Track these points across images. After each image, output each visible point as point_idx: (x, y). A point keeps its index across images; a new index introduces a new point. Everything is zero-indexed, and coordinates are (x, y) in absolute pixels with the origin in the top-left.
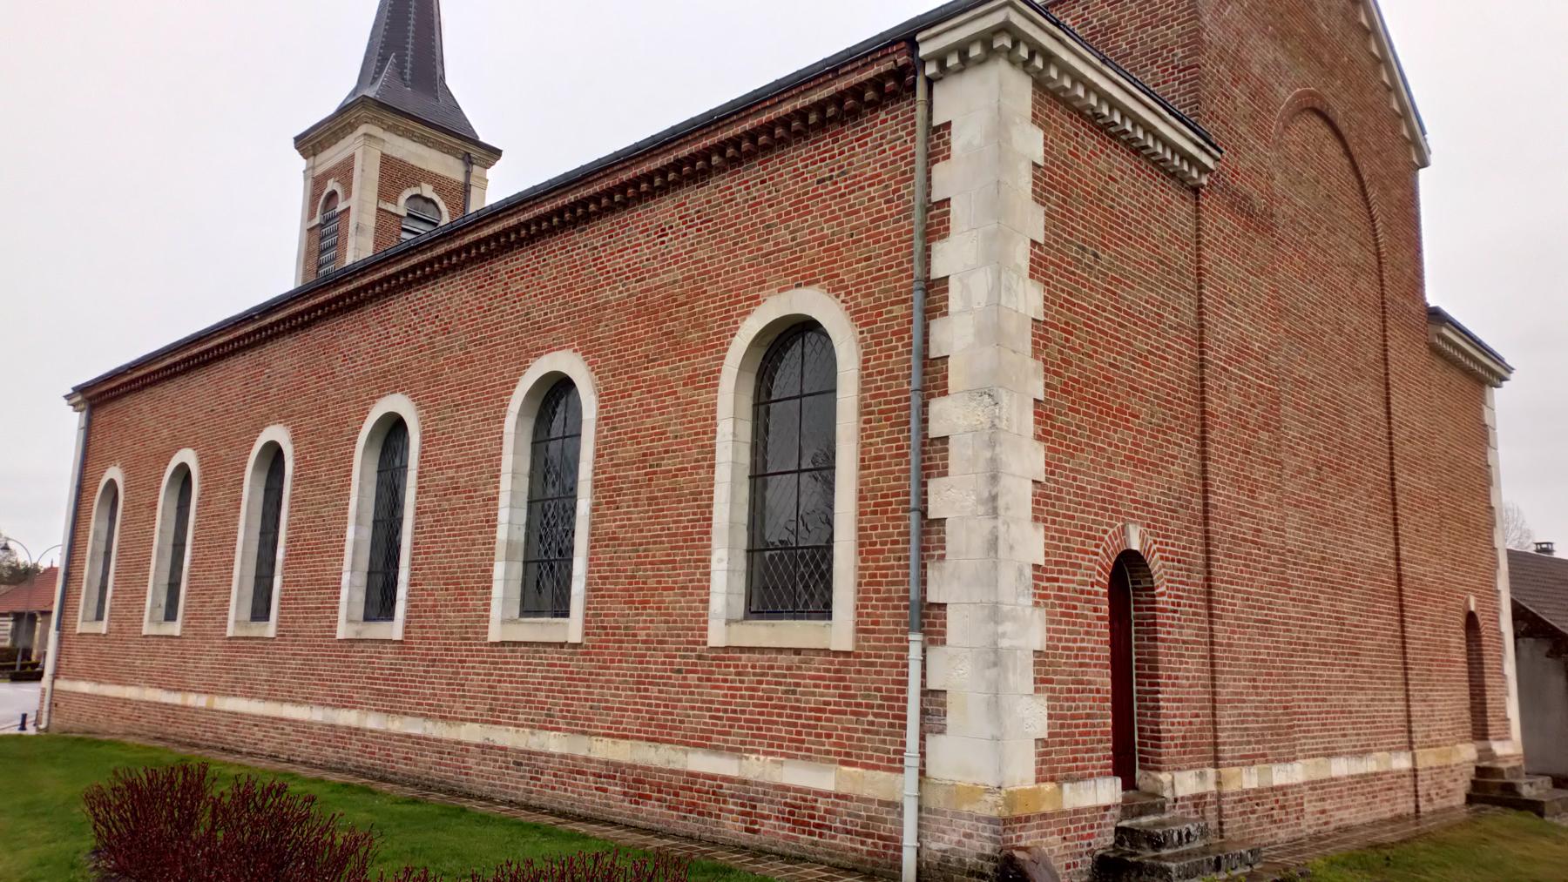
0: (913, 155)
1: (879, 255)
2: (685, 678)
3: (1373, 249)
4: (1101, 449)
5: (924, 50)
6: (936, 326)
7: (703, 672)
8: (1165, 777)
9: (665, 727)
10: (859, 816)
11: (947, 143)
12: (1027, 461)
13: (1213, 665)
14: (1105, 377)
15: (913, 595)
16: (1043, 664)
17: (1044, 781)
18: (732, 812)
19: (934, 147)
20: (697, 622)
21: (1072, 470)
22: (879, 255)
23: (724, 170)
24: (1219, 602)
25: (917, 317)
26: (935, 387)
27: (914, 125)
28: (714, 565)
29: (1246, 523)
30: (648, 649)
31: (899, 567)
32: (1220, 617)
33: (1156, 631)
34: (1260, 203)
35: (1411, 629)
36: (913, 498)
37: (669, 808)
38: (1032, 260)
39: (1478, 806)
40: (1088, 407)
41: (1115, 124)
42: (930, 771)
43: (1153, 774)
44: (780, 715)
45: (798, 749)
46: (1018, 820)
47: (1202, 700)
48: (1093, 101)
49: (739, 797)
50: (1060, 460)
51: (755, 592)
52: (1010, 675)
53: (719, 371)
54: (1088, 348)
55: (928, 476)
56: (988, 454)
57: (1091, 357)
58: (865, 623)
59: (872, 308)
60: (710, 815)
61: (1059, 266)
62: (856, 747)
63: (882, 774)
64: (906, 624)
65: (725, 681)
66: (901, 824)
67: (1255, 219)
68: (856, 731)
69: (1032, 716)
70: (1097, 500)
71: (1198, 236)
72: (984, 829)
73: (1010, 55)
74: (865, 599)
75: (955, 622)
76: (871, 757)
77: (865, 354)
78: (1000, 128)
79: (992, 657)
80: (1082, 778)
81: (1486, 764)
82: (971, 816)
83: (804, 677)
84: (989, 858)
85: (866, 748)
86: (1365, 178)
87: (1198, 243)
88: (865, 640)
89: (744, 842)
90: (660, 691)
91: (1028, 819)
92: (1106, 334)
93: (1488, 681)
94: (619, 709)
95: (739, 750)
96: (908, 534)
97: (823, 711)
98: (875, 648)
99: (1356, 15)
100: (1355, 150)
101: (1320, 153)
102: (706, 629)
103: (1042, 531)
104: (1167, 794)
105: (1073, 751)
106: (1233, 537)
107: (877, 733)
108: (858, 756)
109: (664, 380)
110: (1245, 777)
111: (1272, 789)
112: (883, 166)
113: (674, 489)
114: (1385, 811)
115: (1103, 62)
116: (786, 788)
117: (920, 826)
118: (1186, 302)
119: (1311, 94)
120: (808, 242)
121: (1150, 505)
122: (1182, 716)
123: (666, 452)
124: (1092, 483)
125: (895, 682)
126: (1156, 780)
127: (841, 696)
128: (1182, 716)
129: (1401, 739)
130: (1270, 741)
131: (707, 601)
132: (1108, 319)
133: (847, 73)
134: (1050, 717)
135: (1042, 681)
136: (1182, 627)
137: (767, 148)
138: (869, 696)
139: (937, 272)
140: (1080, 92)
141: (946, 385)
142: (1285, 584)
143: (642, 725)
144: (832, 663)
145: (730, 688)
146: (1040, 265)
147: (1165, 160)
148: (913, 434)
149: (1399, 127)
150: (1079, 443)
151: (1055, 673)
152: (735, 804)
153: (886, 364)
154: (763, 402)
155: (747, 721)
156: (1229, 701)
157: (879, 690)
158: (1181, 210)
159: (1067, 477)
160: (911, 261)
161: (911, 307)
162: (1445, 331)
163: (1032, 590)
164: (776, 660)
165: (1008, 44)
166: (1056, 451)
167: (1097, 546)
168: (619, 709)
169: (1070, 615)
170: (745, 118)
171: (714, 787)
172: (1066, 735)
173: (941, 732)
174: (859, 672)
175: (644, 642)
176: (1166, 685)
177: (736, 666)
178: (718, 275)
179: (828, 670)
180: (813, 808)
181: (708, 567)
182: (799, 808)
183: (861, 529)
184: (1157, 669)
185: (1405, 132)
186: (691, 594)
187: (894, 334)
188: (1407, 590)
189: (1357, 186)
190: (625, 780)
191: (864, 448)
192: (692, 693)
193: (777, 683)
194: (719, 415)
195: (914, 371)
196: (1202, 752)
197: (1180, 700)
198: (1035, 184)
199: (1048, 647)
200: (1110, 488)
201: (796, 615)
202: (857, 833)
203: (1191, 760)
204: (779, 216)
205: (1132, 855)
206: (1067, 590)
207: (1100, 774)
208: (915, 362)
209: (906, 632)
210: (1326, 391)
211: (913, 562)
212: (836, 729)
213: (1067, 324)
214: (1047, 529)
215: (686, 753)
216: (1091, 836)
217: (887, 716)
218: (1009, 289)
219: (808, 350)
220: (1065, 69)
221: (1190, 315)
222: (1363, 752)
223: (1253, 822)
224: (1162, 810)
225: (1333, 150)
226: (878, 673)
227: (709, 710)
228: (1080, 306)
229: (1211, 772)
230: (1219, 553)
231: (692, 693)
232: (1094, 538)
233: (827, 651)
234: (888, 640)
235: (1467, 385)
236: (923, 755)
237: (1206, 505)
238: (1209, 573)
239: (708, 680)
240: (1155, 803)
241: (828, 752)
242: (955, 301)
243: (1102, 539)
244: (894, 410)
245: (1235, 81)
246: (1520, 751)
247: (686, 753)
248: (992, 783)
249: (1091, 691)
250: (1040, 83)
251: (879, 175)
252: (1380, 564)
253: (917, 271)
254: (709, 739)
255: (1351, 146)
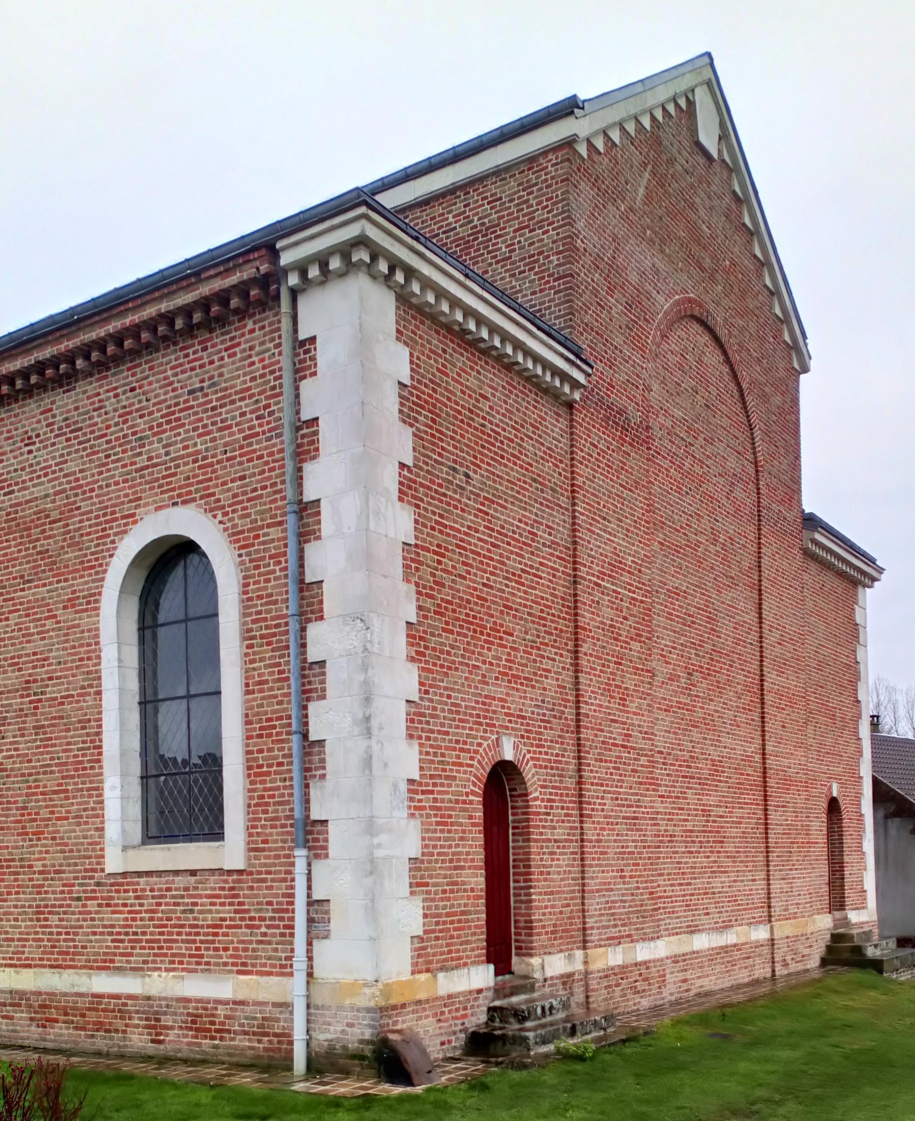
0: (280, 369)
1: (254, 475)
2: (84, 906)
3: (750, 457)
4: (475, 667)
5: (286, 259)
6: (312, 550)
7: (103, 898)
8: (535, 961)
9: (67, 953)
10: (255, 1018)
11: (313, 359)
12: (401, 682)
13: (582, 859)
14: (478, 597)
15: (297, 814)
16: (419, 869)
17: (420, 972)
18: (137, 1026)
19: (300, 362)
20: (94, 850)
21: (446, 689)
22: (254, 475)
23: (91, 375)
24: (589, 803)
25: (292, 541)
26: (312, 612)
27: (280, 337)
28: (107, 793)
29: (617, 729)
30: (45, 879)
31: (285, 787)
32: (590, 816)
33: (529, 833)
34: (635, 416)
35: (773, 817)
36: (294, 721)
37: (76, 1028)
38: (401, 483)
39: (830, 967)
40: (461, 627)
41: (483, 340)
42: (317, 972)
43: (526, 959)
44: (179, 934)
45: (198, 963)
46: (394, 1007)
47: (573, 891)
48: (459, 317)
49: (144, 1012)
50: (434, 679)
51: (152, 818)
52: (387, 883)
53: (100, 594)
54: (461, 570)
55: (308, 700)
56: (362, 678)
57: (464, 578)
58: (256, 842)
59: (249, 530)
60: (117, 1031)
61: (429, 488)
62: (250, 957)
63: (274, 979)
64: (293, 841)
65: (125, 905)
66: (292, 1020)
67: (633, 433)
68: (251, 942)
69: (408, 916)
70: (471, 715)
71: (572, 453)
72: (364, 1018)
73: (370, 268)
74: (255, 819)
75: (336, 836)
76: (265, 965)
77: (245, 578)
78: (363, 343)
79: (368, 867)
80: (457, 967)
81: (841, 931)
82: (352, 1008)
83: (200, 896)
84: (368, 1042)
85: (260, 957)
86: (744, 386)
87: (572, 459)
88: (256, 858)
89: (151, 1052)
90: (61, 920)
91: (403, 1006)
92: (479, 554)
93: (846, 859)
94: (19, 940)
95: (142, 969)
96: (290, 756)
97: (221, 927)
98: (265, 865)
99: (740, 216)
100: (735, 357)
101: (700, 361)
102: (103, 857)
103: (417, 748)
104: (537, 975)
105: (448, 945)
106: (603, 743)
107: (270, 943)
108: (253, 965)
109: (42, 603)
110: (610, 956)
111: (636, 964)
112: (253, 379)
113: (62, 718)
114: (743, 976)
115: (466, 276)
116: (187, 1000)
117: (308, 1021)
118: (560, 520)
119: (690, 300)
120: (182, 457)
121: (524, 718)
122: (553, 907)
123: (50, 679)
124: (466, 700)
125: (284, 895)
126: (528, 964)
127: (236, 912)
128: (553, 907)
129: (762, 913)
130: (635, 924)
131: (102, 829)
132: (480, 540)
133: (211, 277)
134: (425, 916)
135: (417, 886)
136: (554, 828)
137: (135, 353)
138: (260, 910)
139: (309, 495)
140: (445, 307)
141: (321, 610)
142: (654, 783)
143: (44, 953)
144: (226, 882)
145: (129, 912)
146: (410, 488)
147: (537, 376)
148: (292, 659)
149: (780, 331)
150: (453, 662)
151: (430, 876)
152: (140, 1019)
153: (265, 588)
154: (148, 626)
155: (147, 941)
156: (598, 891)
157: (270, 903)
158: (555, 426)
159: (441, 695)
160: (283, 482)
161: (285, 530)
162: (818, 537)
163: (406, 803)
164: (173, 882)
165: (367, 259)
166: (430, 671)
167: (472, 759)
168: (19, 940)
169: (446, 824)
170: (107, 320)
171: (119, 1006)
172: (441, 931)
173: (326, 937)
174: (252, 888)
175: (40, 873)
176: (538, 880)
177: (135, 891)
178: (92, 490)
179: (223, 889)
180: (213, 1015)
181: (101, 795)
182: (201, 1016)
183: (248, 752)
184: (529, 867)
185: (787, 338)
186: (86, 823)
187: (271, 557)
188: (771, 782)
189: (736, 394)
190: (31, 1006)
191: (247, 674)
192: (93, 919)
193: (175, 904)
194: (103, 640)
195: (290, 596)
196: (572, 937)
197: (552, 893)
198: (402, 404)
199: (423, 854)
200: (484, 704)
201: (190, 837)
202: (254, 1034)
203: (561, 944)
204: (151, 428)
205: (501, 1028)
206: (442, 801)
207: (473, 963)
208: (292, 588)
209: (291, 849)
210: (698, 601)
211: (296, 783)
212: (232, 942)
213: (439, 546)
214: (421, 745)
215: (90, 976)
216: (465, 1016)
217: (278, 927)
218: (377, 514)
219: (190, 572)
220: (427, 284)
221: (564, 531)
222: (726, 927)
223: (617, 994)
224: (532, 989)
225: (713, 358)
226: (268, 888)
227: (111, 934)
228: (452, 528)
229: (579, 954)
230: (590, 758)
231: (93, 919)
232: (469, 751)
233: (221, 871)
234: (277, 857)
235: (839, 586)
236: (310, 959)
237: (578, 714)
238: (581, 777)
239: (108, 905)
240: (527, 985)
241: (225, 964)
242: (327, 526)
243: (476, 752)
244: (274, 635)
245: (611, 291)
246: (875, 918)
247: (90, 976)
248: (370, 978)
249: (465, 890)
250: (403, 299)
251: (249, 389)
252: (747, 759)
253: (290, 493)
254: (112, 961)
255: (730, 353)
